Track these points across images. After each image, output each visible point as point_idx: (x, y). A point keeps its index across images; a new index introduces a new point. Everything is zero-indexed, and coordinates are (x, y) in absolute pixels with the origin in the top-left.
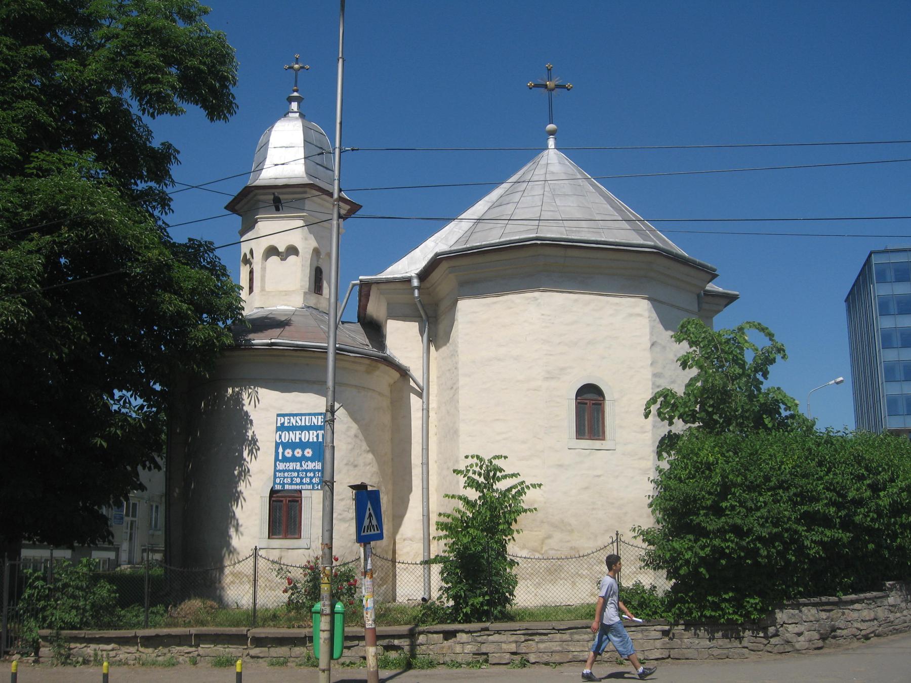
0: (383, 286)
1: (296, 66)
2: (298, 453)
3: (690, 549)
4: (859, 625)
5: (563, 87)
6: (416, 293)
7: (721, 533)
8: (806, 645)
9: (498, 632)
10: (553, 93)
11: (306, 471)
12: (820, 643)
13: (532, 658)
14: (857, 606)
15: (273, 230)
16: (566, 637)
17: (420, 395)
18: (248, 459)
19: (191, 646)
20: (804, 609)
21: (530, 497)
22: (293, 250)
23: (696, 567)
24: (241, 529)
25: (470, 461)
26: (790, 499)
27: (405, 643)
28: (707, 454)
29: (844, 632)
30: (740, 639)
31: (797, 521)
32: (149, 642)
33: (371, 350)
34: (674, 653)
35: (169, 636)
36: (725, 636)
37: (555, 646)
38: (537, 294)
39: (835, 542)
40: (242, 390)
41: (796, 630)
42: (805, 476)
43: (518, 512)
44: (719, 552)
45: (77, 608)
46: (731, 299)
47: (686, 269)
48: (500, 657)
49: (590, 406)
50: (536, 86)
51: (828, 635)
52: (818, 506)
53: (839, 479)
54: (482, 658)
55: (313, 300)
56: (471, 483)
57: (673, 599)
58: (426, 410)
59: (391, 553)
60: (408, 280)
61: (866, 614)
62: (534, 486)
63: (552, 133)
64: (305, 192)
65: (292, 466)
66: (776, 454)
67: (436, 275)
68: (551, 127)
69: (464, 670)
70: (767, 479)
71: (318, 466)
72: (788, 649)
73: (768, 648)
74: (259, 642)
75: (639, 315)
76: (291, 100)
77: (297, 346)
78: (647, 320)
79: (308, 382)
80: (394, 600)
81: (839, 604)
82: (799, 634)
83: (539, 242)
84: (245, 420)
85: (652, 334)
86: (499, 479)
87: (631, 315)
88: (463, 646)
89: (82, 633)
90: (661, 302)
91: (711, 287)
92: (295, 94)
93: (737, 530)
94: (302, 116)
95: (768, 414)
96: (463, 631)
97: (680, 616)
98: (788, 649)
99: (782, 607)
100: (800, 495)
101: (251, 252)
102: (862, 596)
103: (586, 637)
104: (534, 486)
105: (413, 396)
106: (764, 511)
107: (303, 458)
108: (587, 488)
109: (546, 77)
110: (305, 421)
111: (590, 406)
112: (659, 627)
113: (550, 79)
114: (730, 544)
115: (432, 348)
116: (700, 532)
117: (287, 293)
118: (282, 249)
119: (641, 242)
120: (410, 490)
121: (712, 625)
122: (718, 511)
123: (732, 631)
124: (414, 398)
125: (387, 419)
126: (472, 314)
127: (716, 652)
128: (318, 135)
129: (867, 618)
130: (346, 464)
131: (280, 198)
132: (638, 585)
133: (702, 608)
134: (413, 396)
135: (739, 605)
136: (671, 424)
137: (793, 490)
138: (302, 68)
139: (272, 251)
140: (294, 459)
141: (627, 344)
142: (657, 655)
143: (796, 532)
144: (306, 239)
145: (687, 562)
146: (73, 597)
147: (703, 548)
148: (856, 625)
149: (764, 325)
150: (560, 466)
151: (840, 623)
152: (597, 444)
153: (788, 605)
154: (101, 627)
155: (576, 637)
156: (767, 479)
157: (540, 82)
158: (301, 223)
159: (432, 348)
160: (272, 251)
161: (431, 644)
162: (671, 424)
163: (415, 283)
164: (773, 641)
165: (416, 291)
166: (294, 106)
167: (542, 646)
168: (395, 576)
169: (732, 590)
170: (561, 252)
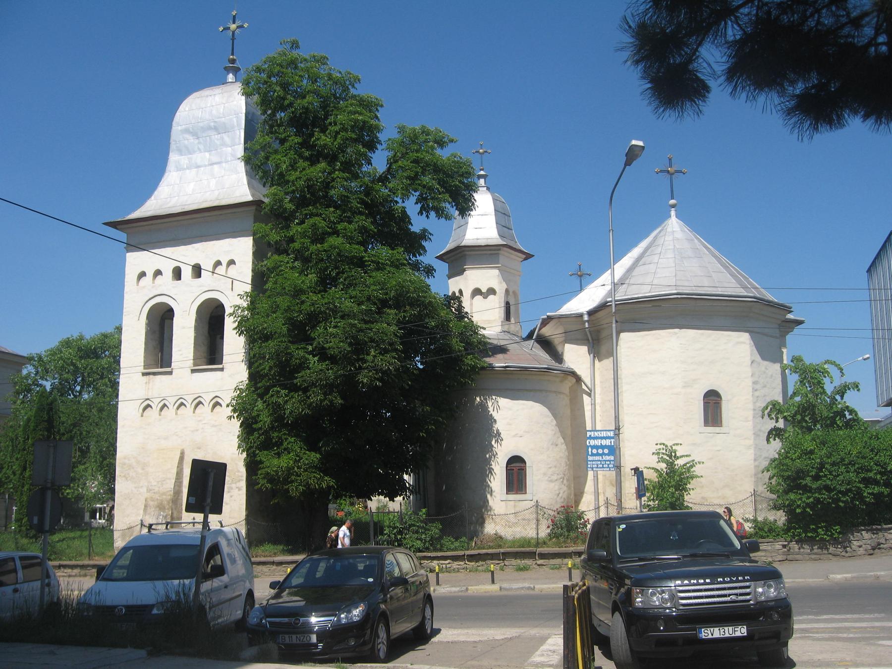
0: (564, 320)
2: (600, 451)
3: (800, 499)
6: (587, 325)
7: (819, 490)
8: (864, 552)
12: (872, 552)
17: (589, 395)
18: (495, 446)
19: (500, 560)
20: (863, 532)
21: (697, 470)
22: (491, 291)
23: (804, 508)
25: (659, 447)
26: (855, 471)
28: (809, 445)
29: (885, 546)
31: (860, 482)
32: (471, 558)
33: (553, 364)
34: (789, 557)
35: (487, 554)
39: (881, 494)
40: (486, 399)
42: (864, 458)
43: (692, 478)
44: (818, 501)
45: (421, 540)
46: (800, 323)
47: (773, 310)
49: (712, 402)
51: (877, 547)
52: (871, 475)
53: (883, 458)
56: (662, 460)
57: (787, 529)
58: (594, 405)
60: (581, 316)
62: (699, 463)
63: (673, 206)
65: (597, 458)
66: (849, 445)
67: (600, 314)
68: (672, 202)
70: (843, 459)
71: (612, 458)
74: (543, 556)
75: (744, 343)
82: (860, 547)
84: (492, 420)
85: (751, 355)
86: (678, 458)
87: (738, 343)
91: (790, 316)
92: (482, 173)
93: (827, 488)
94: (488, 189)
95: (840, 419)
97: (793, 536)
100: (861, 468)
101: (461, 292)
104: (699, 463)
106: (841, 477)
107: (603, 454)
108: (711, 459)
110: (604, 434)
111: (712, 402)
114: (825, 495)
115: (597, 362)
116: (806, 489)
118: (484, 290)
119: (746, 294)
121: (811, 541)
122: (816, 478)
124: (585, 397)
125: (568, 412)
126: (632, 345)
131: (483, 254)
132: (766, 520)
133: (805, 532)
136: (777, 421)
137: (857, 466)
139: (477, 292)
140: (598, 454)
141: (729, 359)
142: (780, 558)
143: (859, 488)
145: (799, 506)
146: (417, 532)
147: (808, 498)
149: (837, 363)
150: (694, 444)
151: (883, 541)
152: (717, 429)
154: (436, 550)
156: (843, 459)
159: (597, 362)
160: (477, 292)
162: (777, 421)
163: (586, 318)
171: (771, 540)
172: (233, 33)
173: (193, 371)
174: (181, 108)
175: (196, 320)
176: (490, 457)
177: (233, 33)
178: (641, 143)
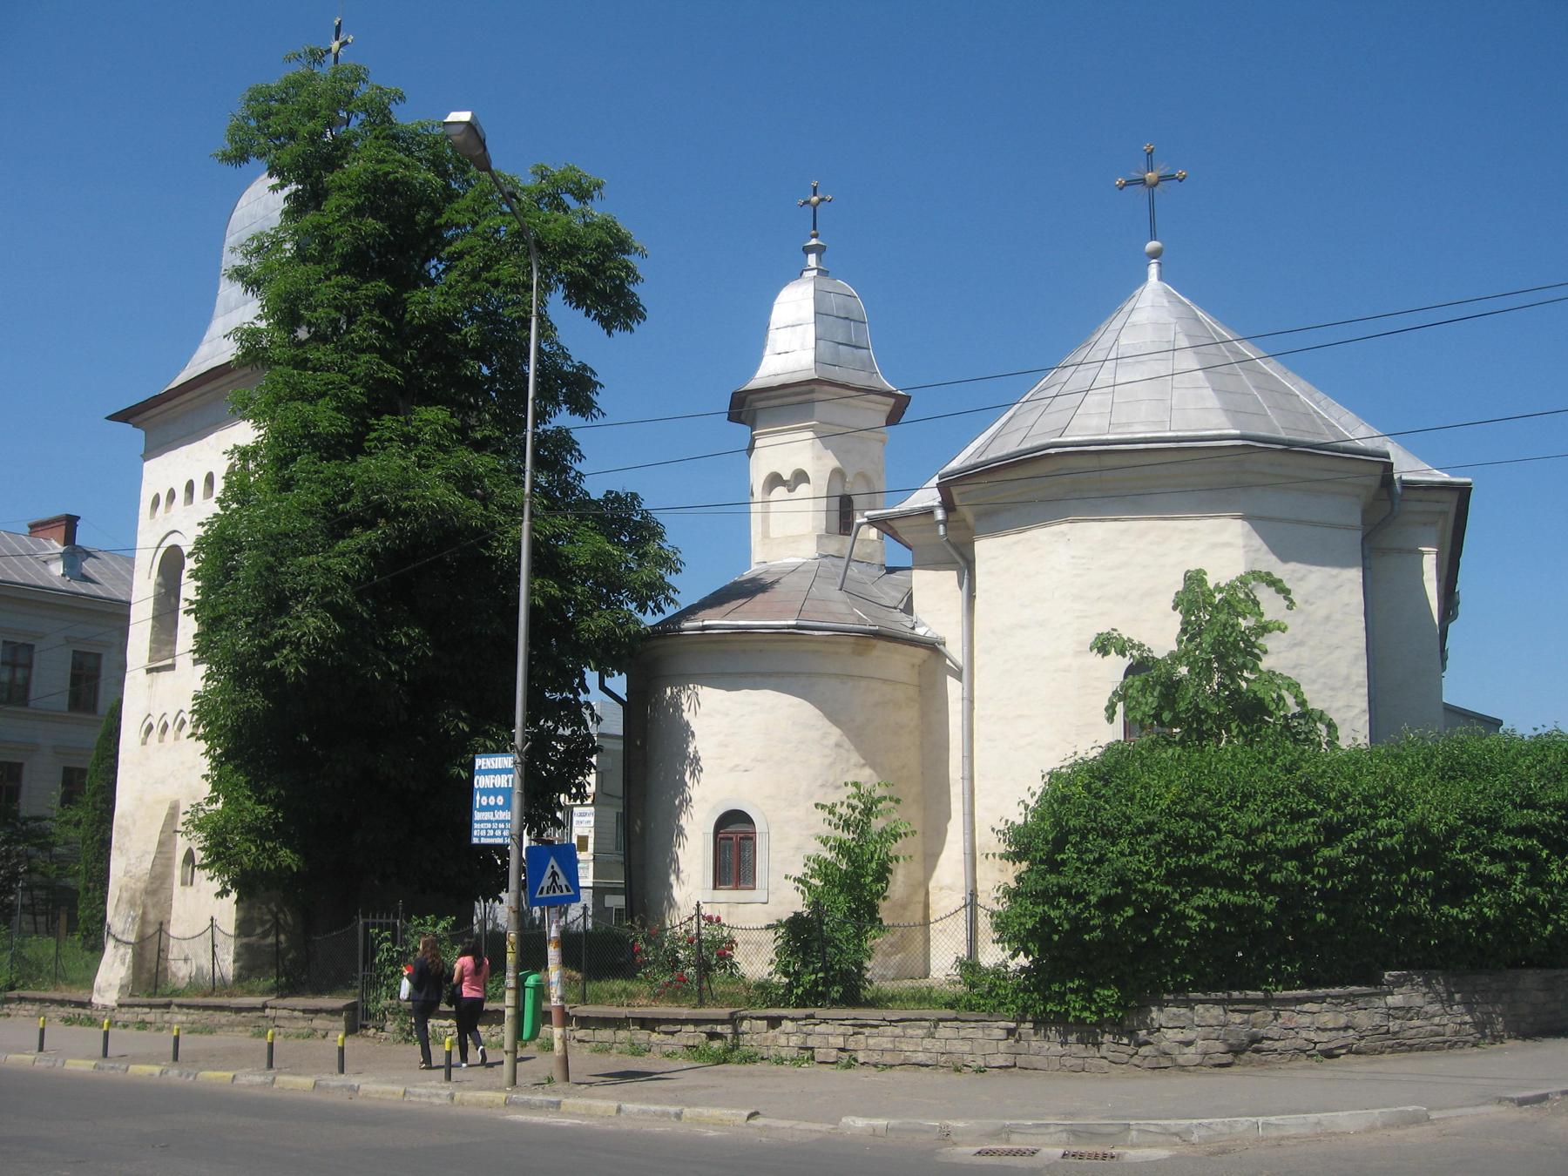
1: (815, 199)
2: (492, 801)
4: (1312, 1036)
5: (1172, 177)
8: (1198, 1059)
9: (825, 1021)
10: (1156, 189)
11: (499, 822)
12: (1228, 1058)
13: (861, 1057)
14: (1307, 1007)
15: (786, 450)
16: (898, 1031)
18: (690, 783)
22: (801, 477)
24: (682, 876)
27: (726, 1029)
29: (1278, 1045)
30: (1098, 1045)
34: (1021, 1061)
36: (1080, 1041)
37: (886, 1043)
38: (1065, 527)
41: (1180, 1037)
48: (827, 1055)
50: (1128, 183)
51: (1244, 1049)
54: (807, 1053)
55: (837, 544)
59: (920, 907)
61: (1327, 1019)
63: (1155, 254)
64: (812, 391)
68: (1152, 245)
69: (785, 1069)
72: (1165, 1062)
73: (1136, 1060)
76: (808, 250)
77: (739, 627)
78: (1242, 551)
79: (762, 674)
80: (927, 976)
81: (1266, 1002)
82: (1189, 1044)
83: (1052, 451)
84: (685, 732)
87: (1214, 546)
88: (787, 1037)
89: (14, 994)
90: (1270, 519)
92: (814, 242)
96: (786, 1018)
98: (1165, 1062)
99: (1161, 1005)
102: (1320, 992)
103: (920, 1032)
105: (949, 678)
109: (1143, 167)
112: (1002, 1024)
113: (1150, 168)
117: (796, 539)
120: (948, 817)
123: (1089, 1035)
127: (1069, 1062)
128: (840, 299)
129: (1330, 1026)
130: (822, 786)
134: (949, 678)
135: (1087, 993)
138: (822, 200)
139: (775, 480)
144: (819, 458)
148: (1304, 1034)
153: (1168, 1001)
155: (910, 1032)
157: (1135, 175)
158: (811, 435)
161: (755, 1033)
164: (1143, 1050)
165: (941, 527)
166: (812, 259)
167: (871, 1041)
168: (927, 940)
169: (1080, 976)
170: (1093, 462)
171: (984, 1015)
172: (336, 55)
173: (149, 671)
174: (243, 202)
175: (994, 536)
176: (681, 803)
177: (336, 55)
178: (465, 116)
